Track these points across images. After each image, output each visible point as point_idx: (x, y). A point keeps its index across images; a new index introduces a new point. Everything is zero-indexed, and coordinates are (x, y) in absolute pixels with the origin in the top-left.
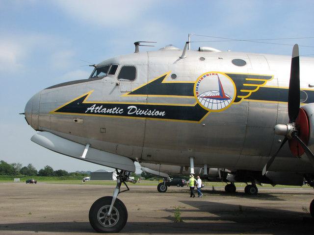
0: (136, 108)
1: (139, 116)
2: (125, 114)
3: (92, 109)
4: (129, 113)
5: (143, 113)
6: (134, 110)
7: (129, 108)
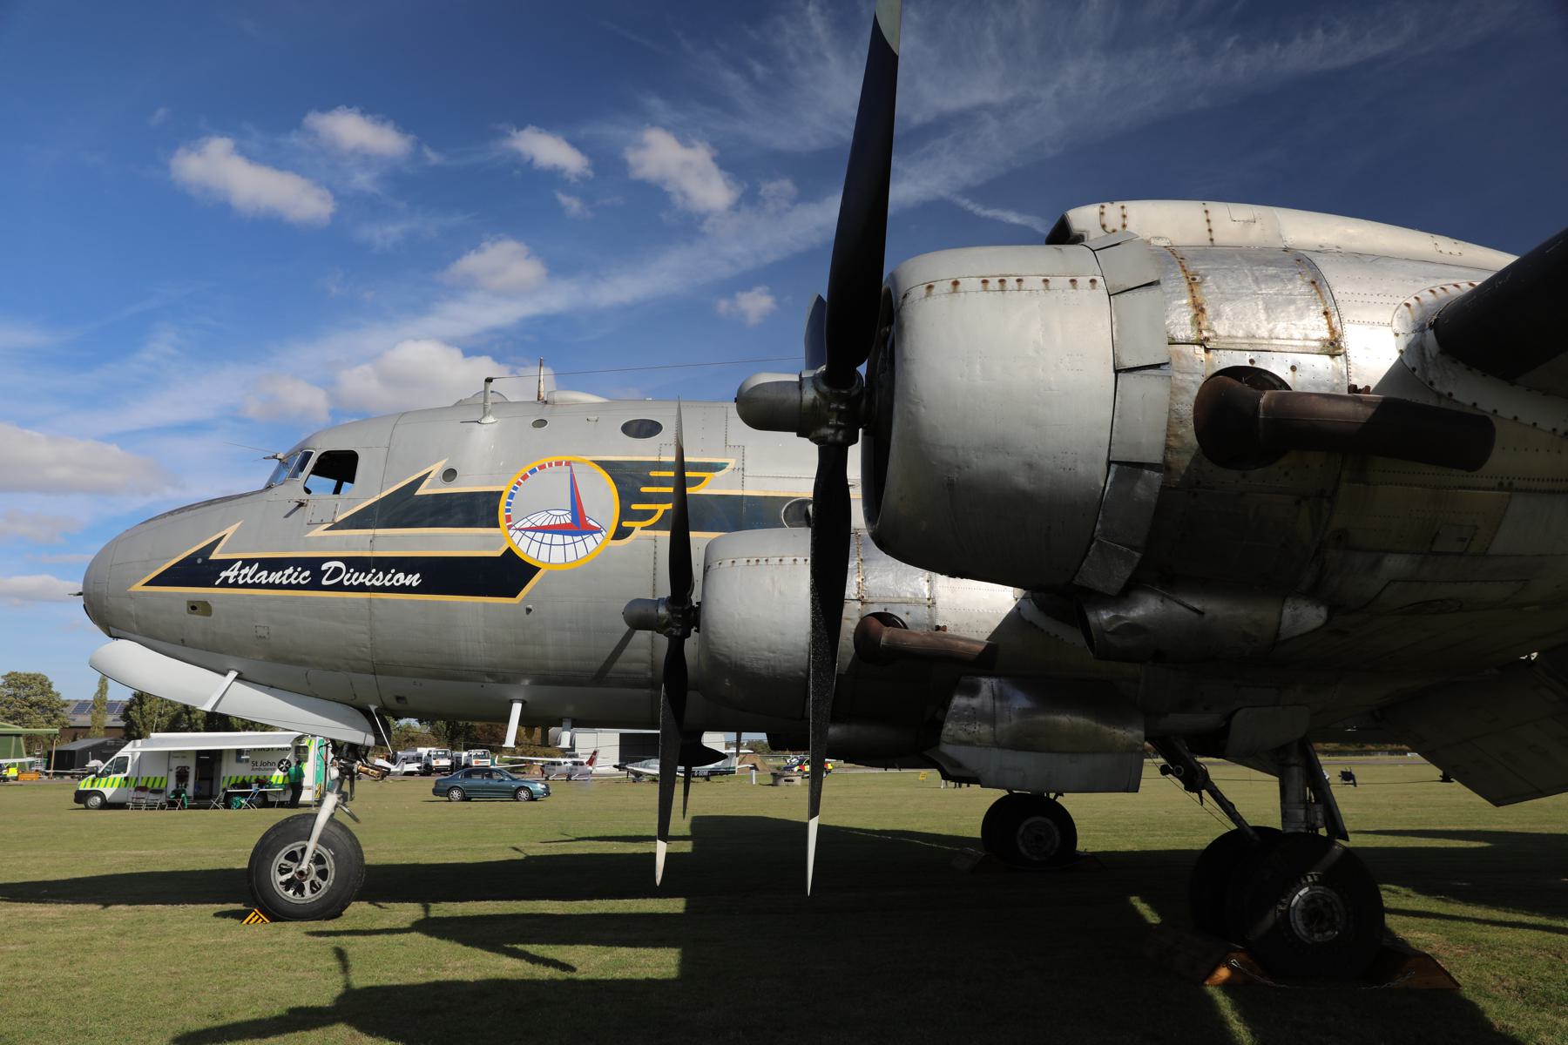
0: (341, 565)
1: (351, 588)
2: (314, 585)
3: (230, 574)
4: (325, 582)
5: (361, 580)
6: (337, 571)
7: (324, 567)
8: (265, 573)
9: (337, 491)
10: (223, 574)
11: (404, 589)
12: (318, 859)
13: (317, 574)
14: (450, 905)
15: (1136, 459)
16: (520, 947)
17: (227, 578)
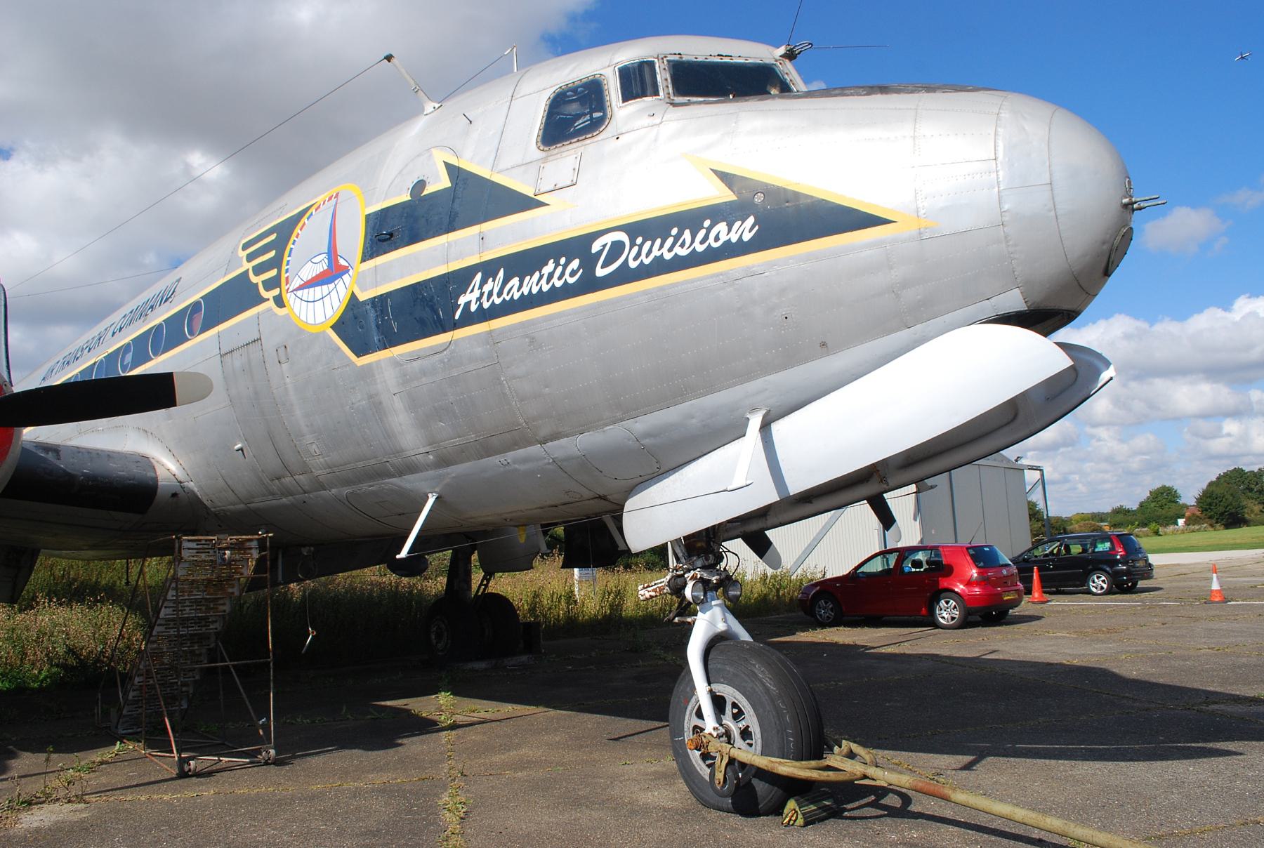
0: (622, 237)
1: (644, 272)
2: (589, 284)
3: (469, 298)
4: (600, 272)
5: (656, 253)
6: (617, 248)
7: (596, 247)
8: (515, 281)
9: (421, 184)
10: (462, 300)
11: (739, 249)
12: (719, 703)
13: (589, 262)
14: (816, 640)
15: (878, 98)
16: (1211, 745)
17: (468, 304)
